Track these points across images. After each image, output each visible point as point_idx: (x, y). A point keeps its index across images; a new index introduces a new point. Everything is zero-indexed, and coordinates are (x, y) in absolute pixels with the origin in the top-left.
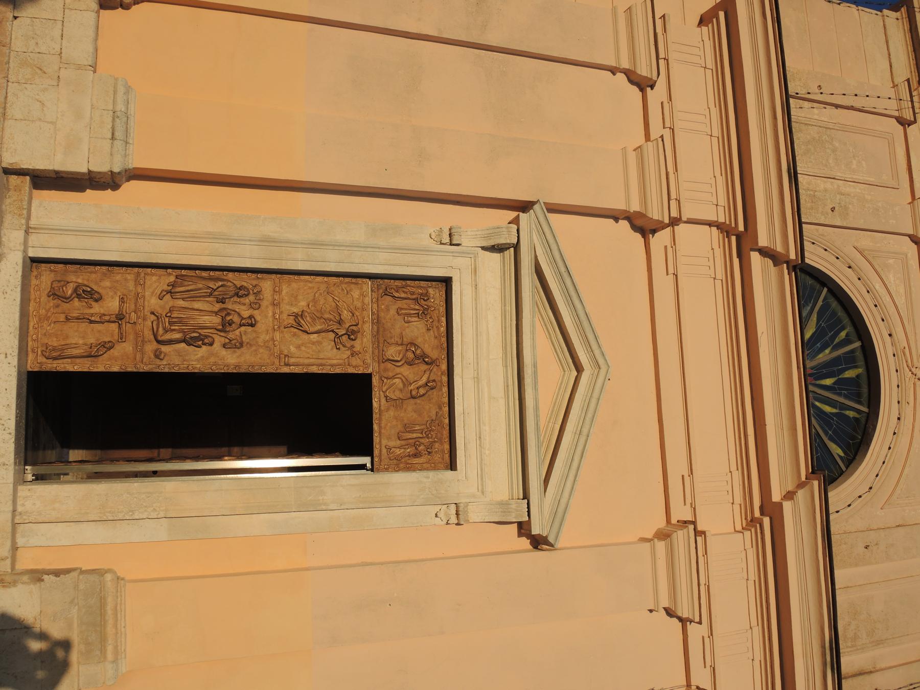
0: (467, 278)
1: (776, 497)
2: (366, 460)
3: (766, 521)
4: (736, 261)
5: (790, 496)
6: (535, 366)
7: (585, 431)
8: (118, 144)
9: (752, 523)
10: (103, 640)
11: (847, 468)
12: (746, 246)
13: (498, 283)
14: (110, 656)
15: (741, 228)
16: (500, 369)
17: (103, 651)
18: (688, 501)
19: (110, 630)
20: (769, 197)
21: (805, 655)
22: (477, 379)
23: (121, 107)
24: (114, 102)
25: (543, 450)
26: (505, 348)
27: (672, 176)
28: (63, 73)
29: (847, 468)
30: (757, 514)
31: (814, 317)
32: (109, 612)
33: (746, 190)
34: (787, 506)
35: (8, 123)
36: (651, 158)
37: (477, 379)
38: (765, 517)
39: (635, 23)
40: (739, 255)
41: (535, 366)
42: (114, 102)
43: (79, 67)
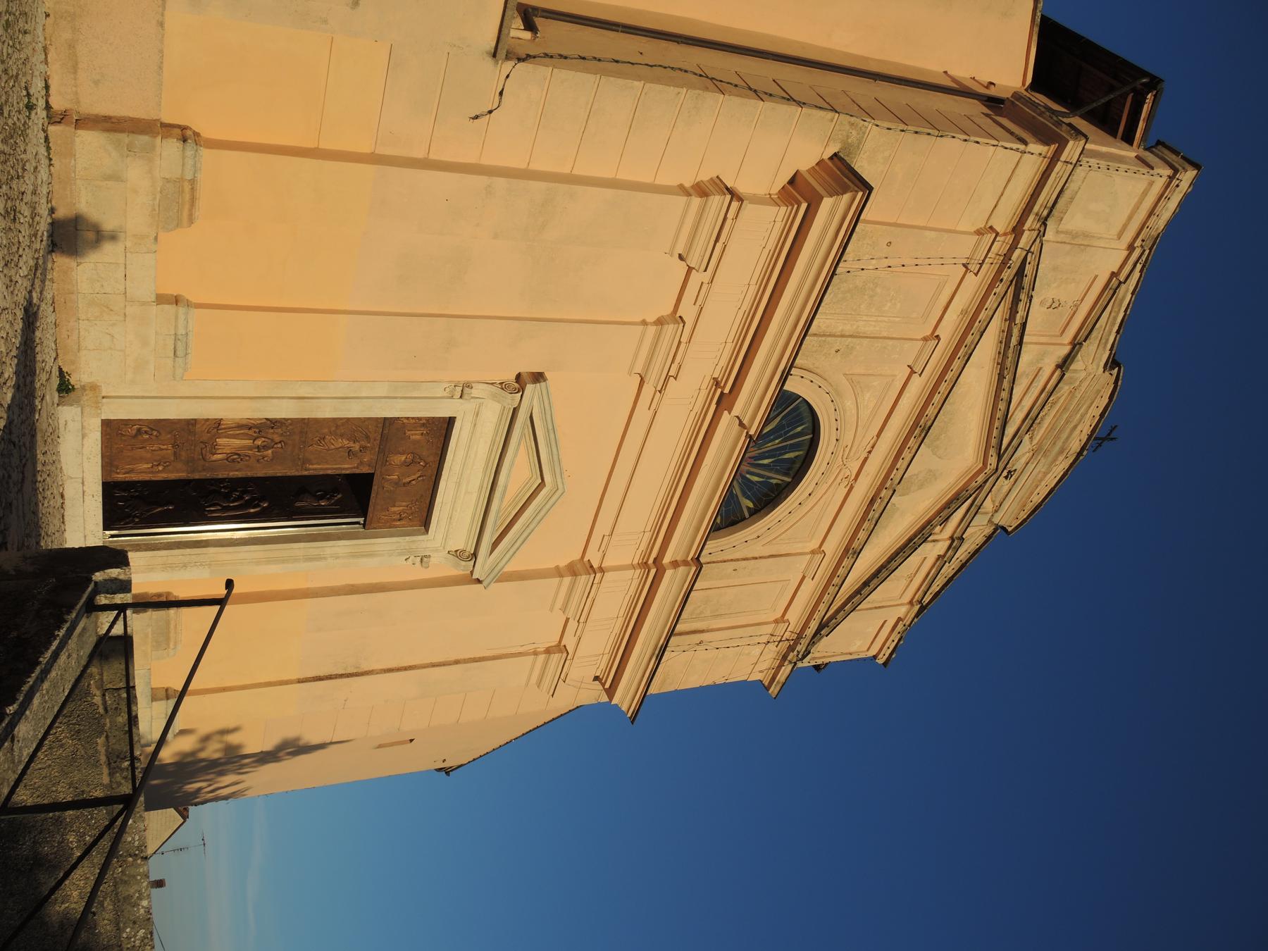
0: (468, 427)
1: (667, 560)
2: (361, 520)
3: (653, 571)
4: (713, 406)
5: (675, 564)
6: (506, 487)
7: (532, 527)
8: (180, 361)
9: (644, 565)
10: (168, 639)
11: (751, 515)
12: (724, 403)
13: (495, 420)
14: (172, 646)
15: (727, 391)
16: (480, 475)
17: (168, 645)
18: (699, 303)
19: (172, 635)
20: (758, 381)
21: (644, 644)
22: (459, 484)
23: (181, 331)
24: (176, 327)
25: (499, 523)
26: (491, 451)
27: (729, 222)
28: (129, 310)
29: (751, 515)
30: (651, 561)
31: (779, 419)
32: (172, 626)
33: (781, 281)
34: (669, 573)
35: (83, 353)
36: (711, 215)
37: (459, 484)
38: (654, 568)
39: (705, 215)
40: (718, 403)
41: (506, 487)
42: (176, 327)
43: (144, 304)
